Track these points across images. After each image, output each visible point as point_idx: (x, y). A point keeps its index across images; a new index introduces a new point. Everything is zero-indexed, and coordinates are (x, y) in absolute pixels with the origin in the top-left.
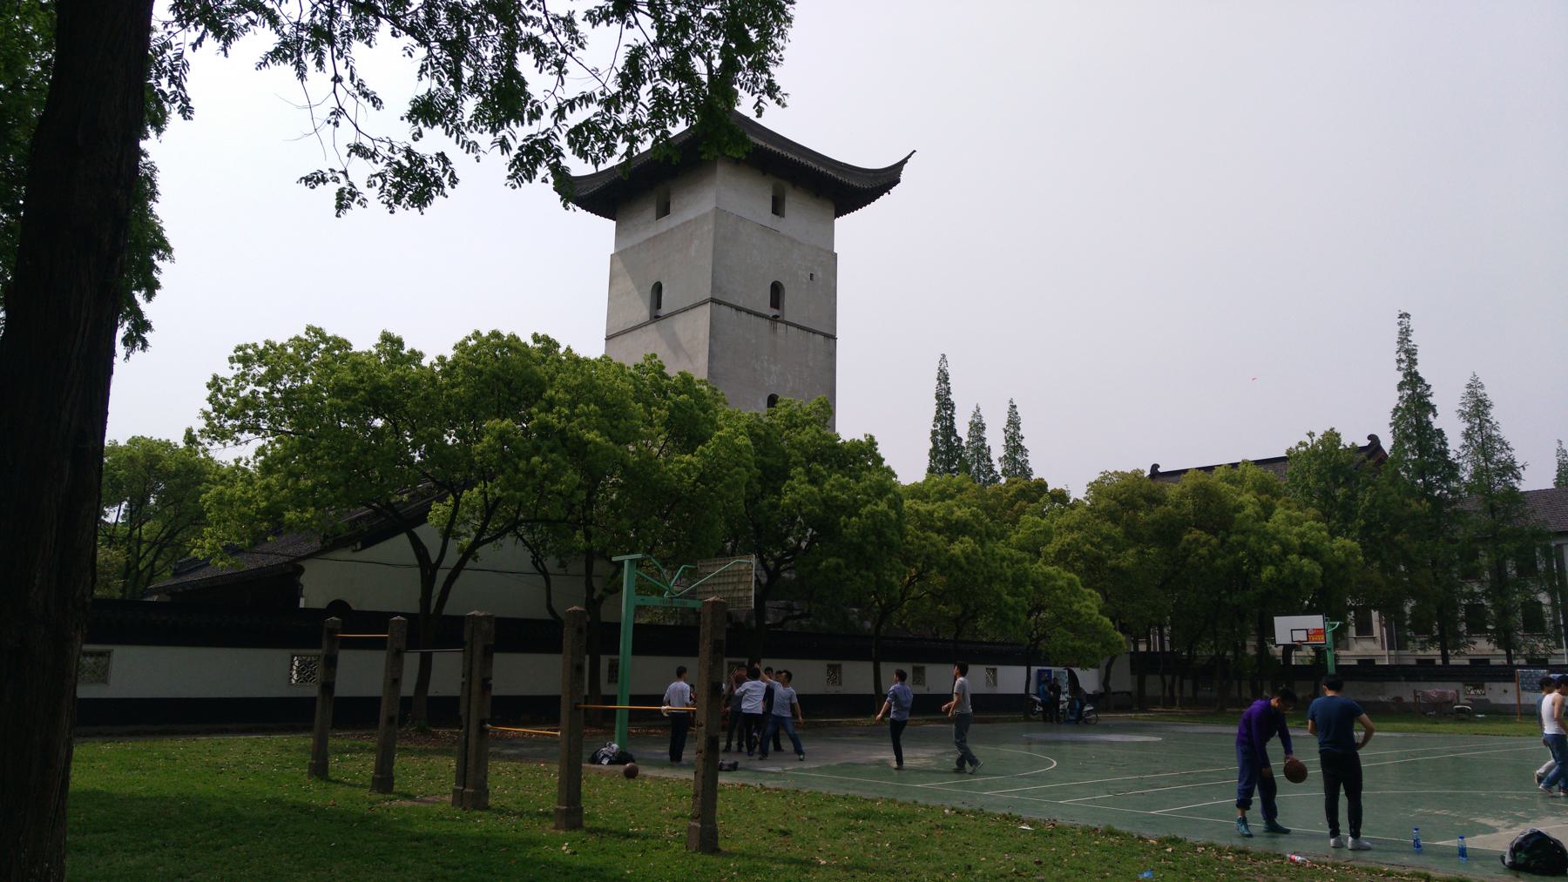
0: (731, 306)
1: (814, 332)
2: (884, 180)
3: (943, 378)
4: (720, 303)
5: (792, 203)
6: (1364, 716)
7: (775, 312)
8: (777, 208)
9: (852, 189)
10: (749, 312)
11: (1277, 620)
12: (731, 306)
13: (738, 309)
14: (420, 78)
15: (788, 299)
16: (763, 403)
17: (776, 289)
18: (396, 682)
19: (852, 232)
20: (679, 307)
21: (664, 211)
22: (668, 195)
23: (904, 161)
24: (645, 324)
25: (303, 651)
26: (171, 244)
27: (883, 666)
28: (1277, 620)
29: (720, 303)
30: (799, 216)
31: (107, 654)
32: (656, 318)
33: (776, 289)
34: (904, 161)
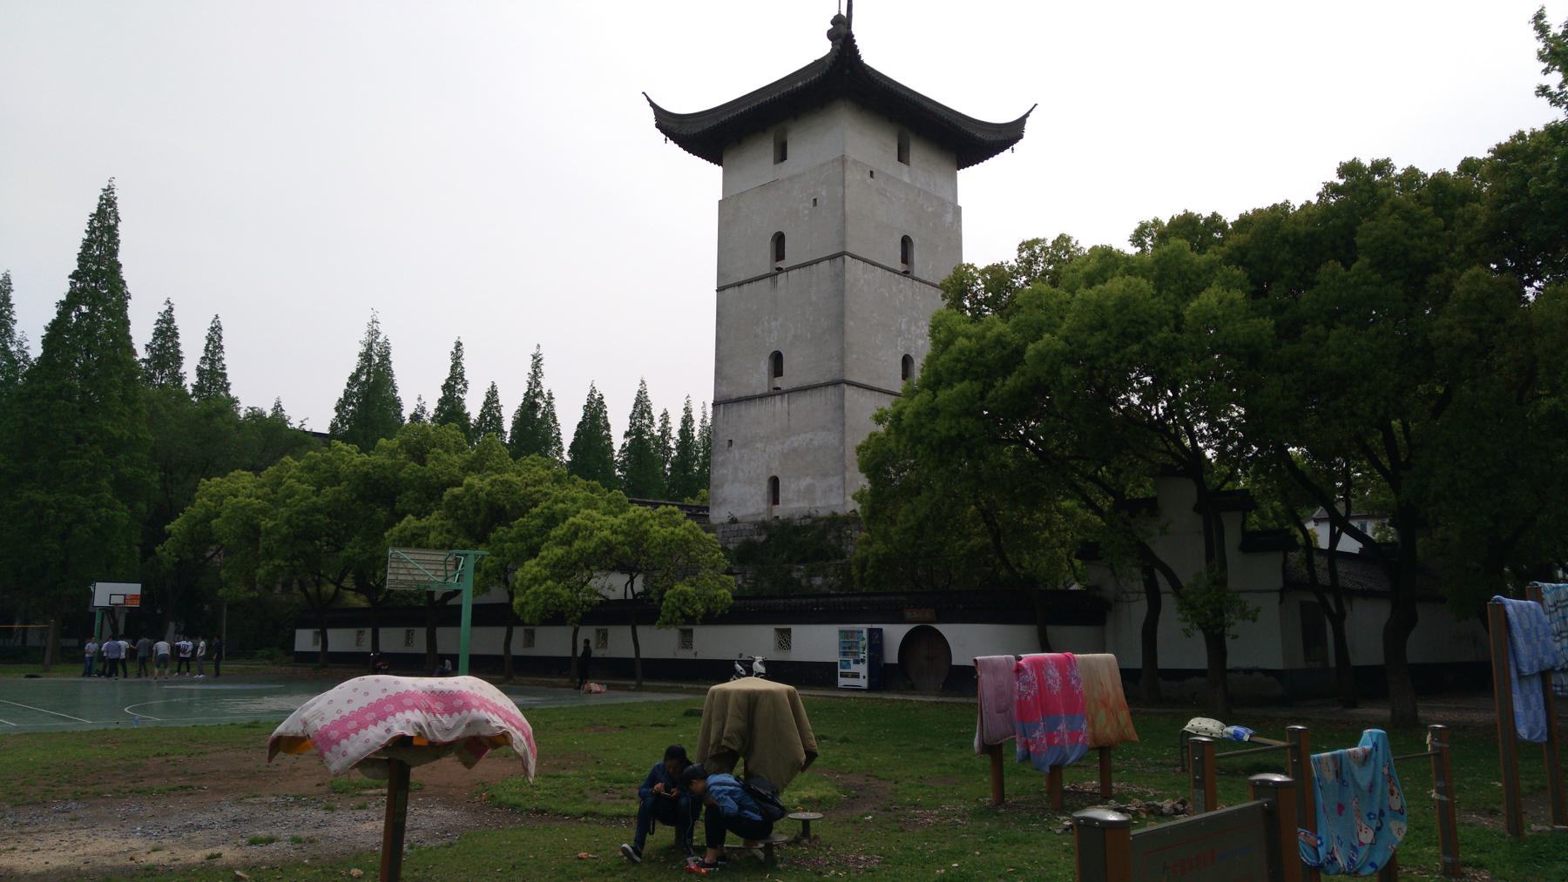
0: (733, 286)
2: (1006, 136)
3: (537, 362)
5: (917, 153)
6: (202, 644)
8: (903, 157)
10: (750, 281)
12: (733, 286)
13: (740, 284)
15: (917, 256)
16: (765, 366)
17: (906, 242)
18: (575, 649)
19: (971, 180)
22: (785, 132)
23: (1027, 115)
24: (934, 285)
26: (1137, 226)
27: (381, 630)
30: (922, 167)
33: (906, 242)
34: (1027, 115)
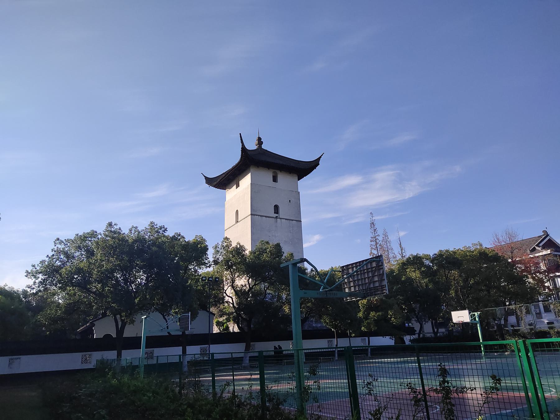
0: (259, 216)
1: (292, 220)
4: (254, 215)
7: (277, 215)
8: (275, 179)
9: (302, 169)
11: (453, 313)
12: (259, 216)
13: (261, 216)
14: (225, 181)
15: (281, 210)
19: (307, 186)
20: (399, 246)
21: (238, 186)
23: (320, 157)
25: (314, 280)
28: (453, 313)
29: (254, 215)
31: (20, 358)
32: (237, 222)
34: (320, 157)
